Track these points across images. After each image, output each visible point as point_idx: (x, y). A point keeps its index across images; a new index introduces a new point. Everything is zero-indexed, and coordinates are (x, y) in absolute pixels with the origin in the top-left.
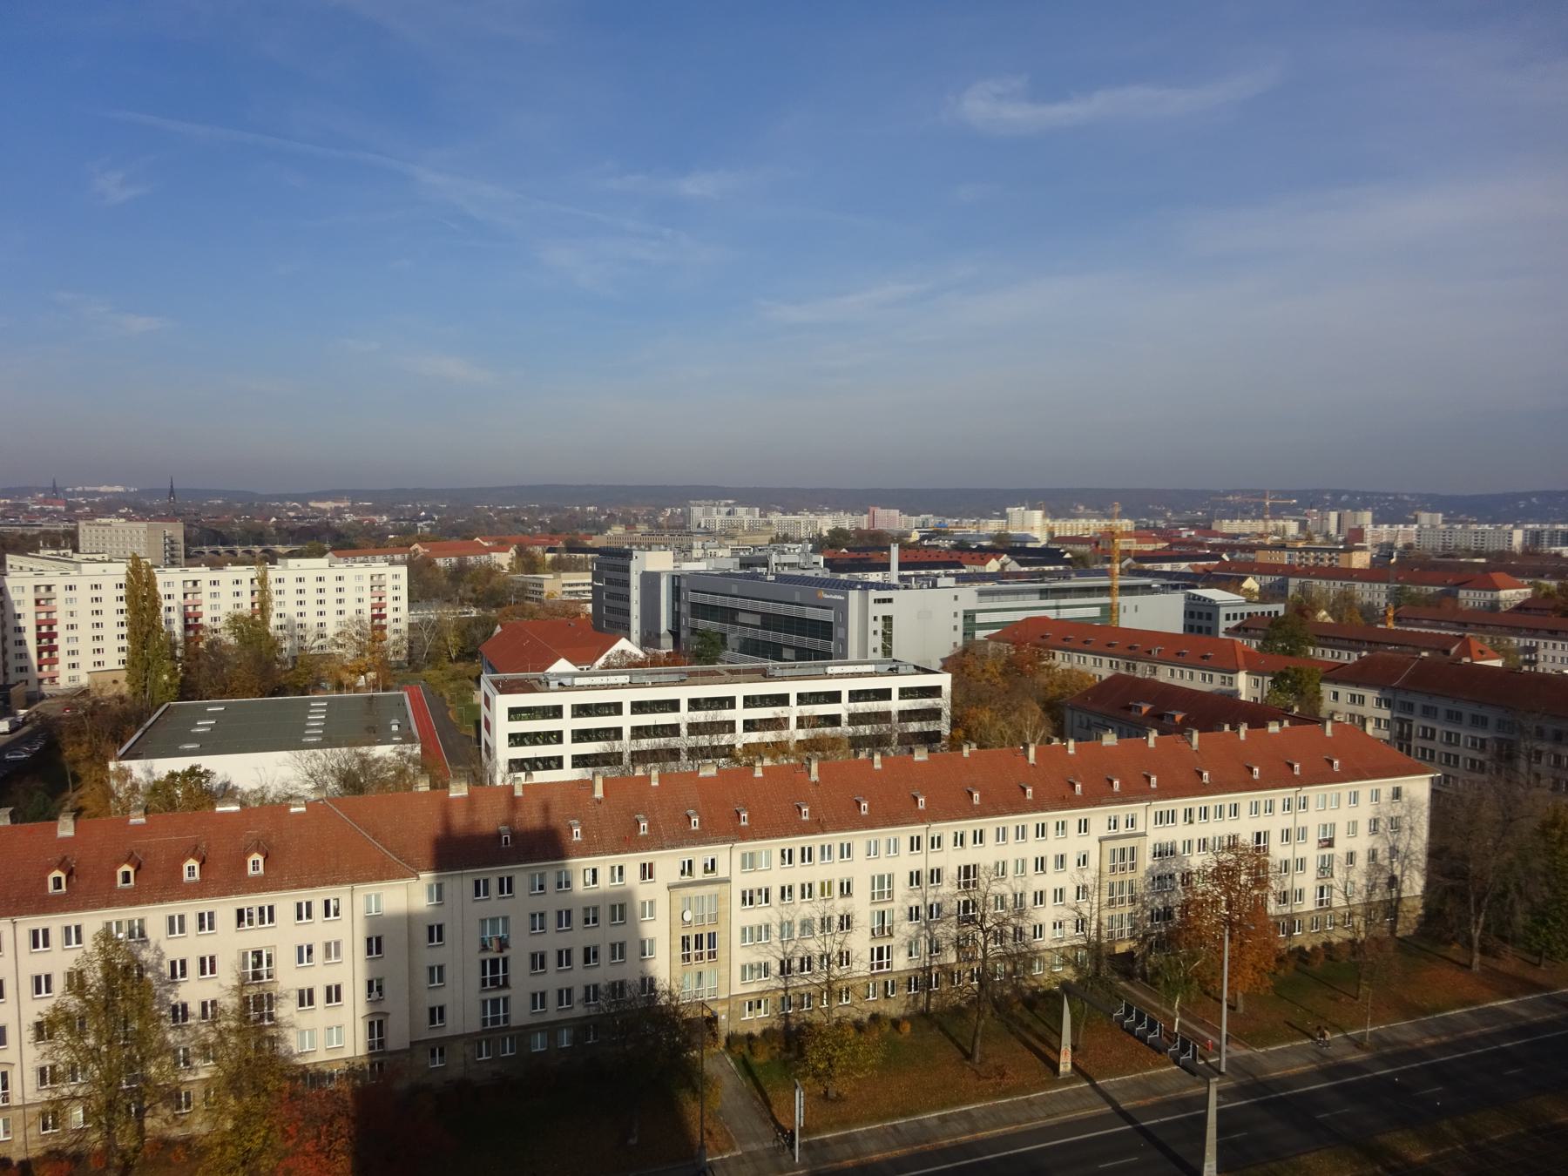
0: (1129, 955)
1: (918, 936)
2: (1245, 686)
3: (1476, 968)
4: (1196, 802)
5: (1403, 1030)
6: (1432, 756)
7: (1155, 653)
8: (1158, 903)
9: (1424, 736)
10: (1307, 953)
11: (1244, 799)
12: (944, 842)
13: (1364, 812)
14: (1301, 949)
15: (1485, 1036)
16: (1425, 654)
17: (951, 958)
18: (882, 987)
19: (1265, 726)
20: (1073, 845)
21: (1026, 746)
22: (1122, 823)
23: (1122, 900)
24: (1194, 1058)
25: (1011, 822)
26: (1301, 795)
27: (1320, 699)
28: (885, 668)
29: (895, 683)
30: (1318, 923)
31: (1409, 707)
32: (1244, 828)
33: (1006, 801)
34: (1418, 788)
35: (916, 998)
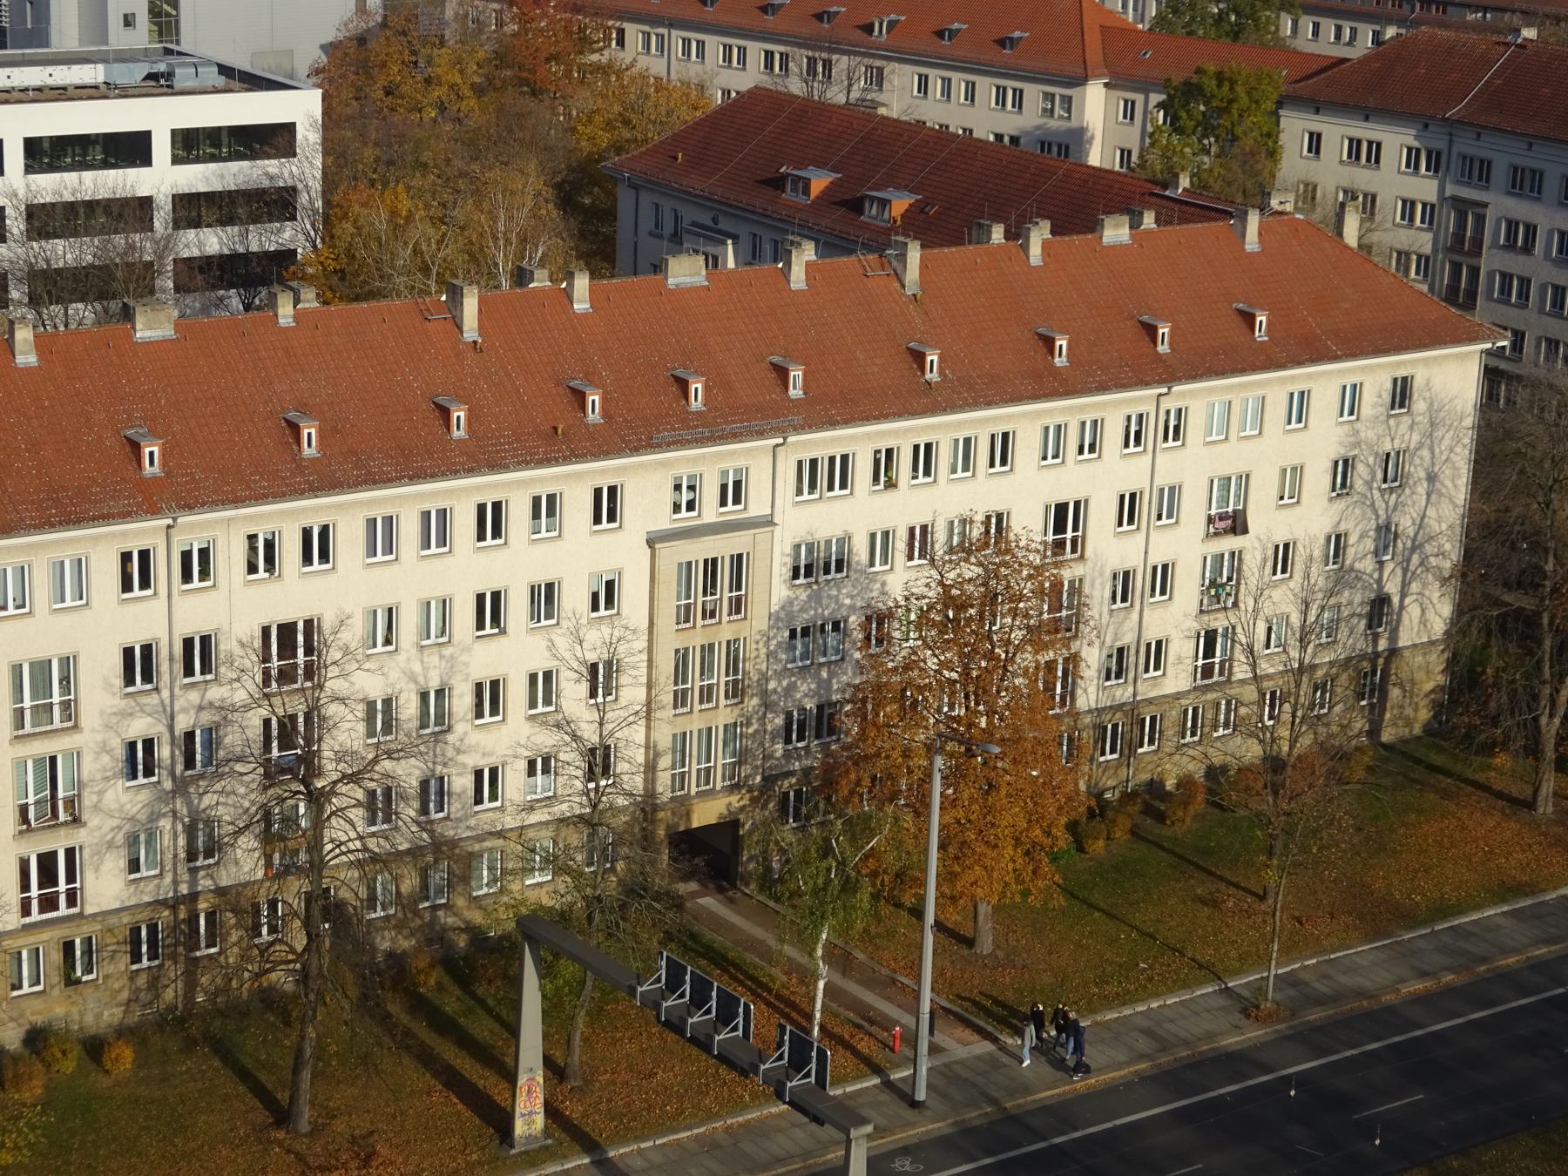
0: (729, 827)
1: (154, 817)
2: (1103, 122)
3: (1546, 807)
4: (903, 433)
5: (1365, 966)
6: (1524, 294)
7: (881, 33)
8: (805, 696)
9: (1510, 245)
10: (1165, 796)
11: (1027, 421)
12: (219, 562)
13: (1323, 440)
14: (1154, 787)
15: (1539, 966)
16: (1529, 33)
17: (245, 863)
18: (57, 957)
19: (1094, 226)
20: (578, 554)
21: (456, 295)
22: (710, 493)
23: (707, 694)
24: (821, 1081)
25: (406, 502)
26: (1170, 404)
27: (1273, 154)
28: (136, 73)
29: (160, 117)
30: (1193, 722)
31: (1479, 172)
32: (1023, 497)
33: (393, 444)
34: (1453, 377)
35: (155, 982)
